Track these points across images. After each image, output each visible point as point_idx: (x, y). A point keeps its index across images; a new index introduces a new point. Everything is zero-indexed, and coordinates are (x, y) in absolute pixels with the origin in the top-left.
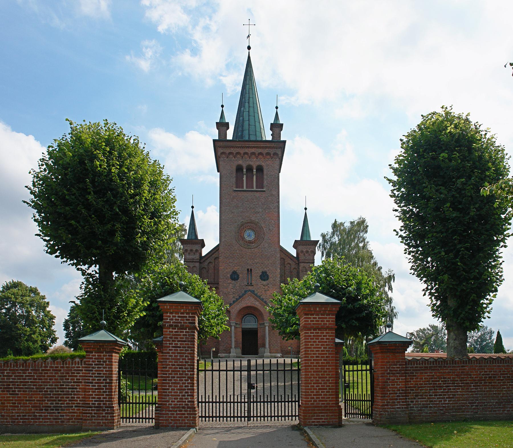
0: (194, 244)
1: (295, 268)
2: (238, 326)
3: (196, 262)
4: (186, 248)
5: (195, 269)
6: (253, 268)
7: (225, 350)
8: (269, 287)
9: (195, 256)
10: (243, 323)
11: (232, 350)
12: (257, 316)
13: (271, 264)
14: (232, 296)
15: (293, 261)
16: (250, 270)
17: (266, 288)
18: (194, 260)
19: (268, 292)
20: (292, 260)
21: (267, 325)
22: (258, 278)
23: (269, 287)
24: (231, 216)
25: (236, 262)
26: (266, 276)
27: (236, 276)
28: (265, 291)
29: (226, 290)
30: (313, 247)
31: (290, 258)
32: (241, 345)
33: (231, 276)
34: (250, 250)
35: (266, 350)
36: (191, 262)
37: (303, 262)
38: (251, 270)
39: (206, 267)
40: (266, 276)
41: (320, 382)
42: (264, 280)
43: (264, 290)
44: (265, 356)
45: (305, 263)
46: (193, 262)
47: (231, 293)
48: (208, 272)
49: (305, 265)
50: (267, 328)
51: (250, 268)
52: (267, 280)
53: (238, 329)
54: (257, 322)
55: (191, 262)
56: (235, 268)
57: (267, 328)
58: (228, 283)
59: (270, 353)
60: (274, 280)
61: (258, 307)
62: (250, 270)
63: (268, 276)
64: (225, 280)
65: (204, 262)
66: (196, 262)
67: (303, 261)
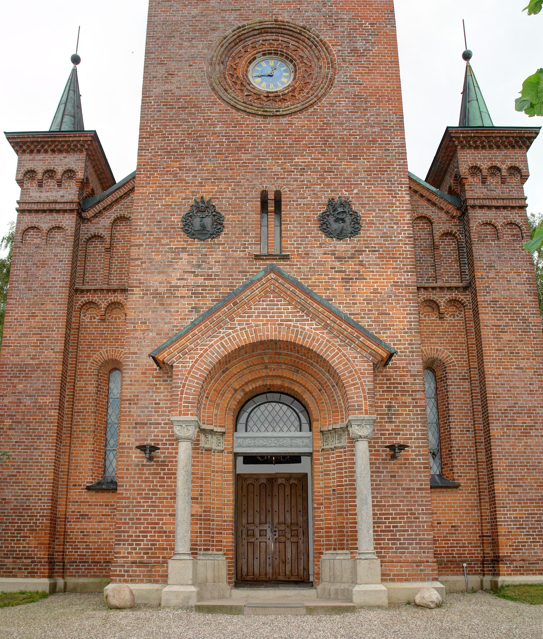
0: (60, 151)
1: (447, 234)
2: (212, 442)
3: (65, 211)
4: (29, 166)
5: (58, 236)
6: (285, 190)
7: (142, 564)
8: (361, 264)
9: (61, 193)
10: (241, 433)
11: (173, 566)
12: (307, 397)
13: (368, 171)
14: (185, 305)
15: (441, 209)
16: (271, 208)
17: (350, 266)
18: (58, 207)
19: (360, 284)
20: (434, 204)
21: (366, 431)
22: (314, 226)
23: (361, 264)
24: (194, 12)
25: (211, 166)
26: (348, 219)
27: (208, 221)
28: (346, 280)
29: (161, 278)
30: (517, 152)
31: (429, 200)
32: (228, 539)
33: (187, 220)
34: (274, 120)
35: (362, 567)
36: (44, 211)
37: (481, 207)
38: (278, 195)
39: (106, 234)
40: (348, 219)
41: (144, 484)
42: (340, 236)
43: (337, 276)
44: (357, 600)
45: (489, 207)
46: (51, 211)
47: (184, 292)
48: (108, 250)
49: (490, 215)
50: (362, 447)
51: (272, 189)
52: (355, 232)
53: (215, 458)
54: (306, 426)
55: (44, 211)
56: (208, 188)
57: (362, 447)
58: (171, 251)
59: (385, 577)
60: (385, 236)
61: (315, 347)
62: (271, 208)
63: (356, 221)
64: (158, 240)
65: (95, 216)
66: (65, 211)
67: (482, 202)
